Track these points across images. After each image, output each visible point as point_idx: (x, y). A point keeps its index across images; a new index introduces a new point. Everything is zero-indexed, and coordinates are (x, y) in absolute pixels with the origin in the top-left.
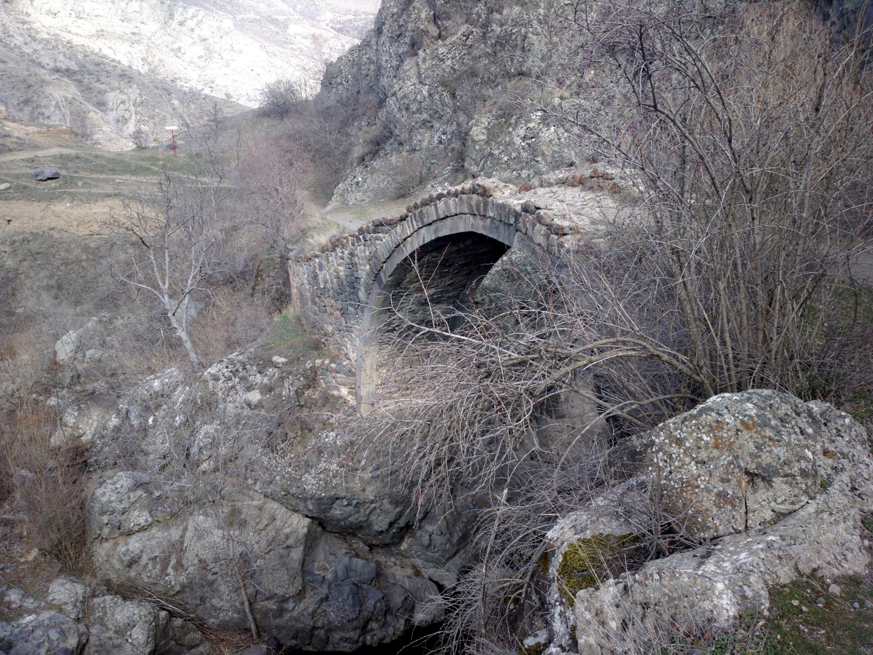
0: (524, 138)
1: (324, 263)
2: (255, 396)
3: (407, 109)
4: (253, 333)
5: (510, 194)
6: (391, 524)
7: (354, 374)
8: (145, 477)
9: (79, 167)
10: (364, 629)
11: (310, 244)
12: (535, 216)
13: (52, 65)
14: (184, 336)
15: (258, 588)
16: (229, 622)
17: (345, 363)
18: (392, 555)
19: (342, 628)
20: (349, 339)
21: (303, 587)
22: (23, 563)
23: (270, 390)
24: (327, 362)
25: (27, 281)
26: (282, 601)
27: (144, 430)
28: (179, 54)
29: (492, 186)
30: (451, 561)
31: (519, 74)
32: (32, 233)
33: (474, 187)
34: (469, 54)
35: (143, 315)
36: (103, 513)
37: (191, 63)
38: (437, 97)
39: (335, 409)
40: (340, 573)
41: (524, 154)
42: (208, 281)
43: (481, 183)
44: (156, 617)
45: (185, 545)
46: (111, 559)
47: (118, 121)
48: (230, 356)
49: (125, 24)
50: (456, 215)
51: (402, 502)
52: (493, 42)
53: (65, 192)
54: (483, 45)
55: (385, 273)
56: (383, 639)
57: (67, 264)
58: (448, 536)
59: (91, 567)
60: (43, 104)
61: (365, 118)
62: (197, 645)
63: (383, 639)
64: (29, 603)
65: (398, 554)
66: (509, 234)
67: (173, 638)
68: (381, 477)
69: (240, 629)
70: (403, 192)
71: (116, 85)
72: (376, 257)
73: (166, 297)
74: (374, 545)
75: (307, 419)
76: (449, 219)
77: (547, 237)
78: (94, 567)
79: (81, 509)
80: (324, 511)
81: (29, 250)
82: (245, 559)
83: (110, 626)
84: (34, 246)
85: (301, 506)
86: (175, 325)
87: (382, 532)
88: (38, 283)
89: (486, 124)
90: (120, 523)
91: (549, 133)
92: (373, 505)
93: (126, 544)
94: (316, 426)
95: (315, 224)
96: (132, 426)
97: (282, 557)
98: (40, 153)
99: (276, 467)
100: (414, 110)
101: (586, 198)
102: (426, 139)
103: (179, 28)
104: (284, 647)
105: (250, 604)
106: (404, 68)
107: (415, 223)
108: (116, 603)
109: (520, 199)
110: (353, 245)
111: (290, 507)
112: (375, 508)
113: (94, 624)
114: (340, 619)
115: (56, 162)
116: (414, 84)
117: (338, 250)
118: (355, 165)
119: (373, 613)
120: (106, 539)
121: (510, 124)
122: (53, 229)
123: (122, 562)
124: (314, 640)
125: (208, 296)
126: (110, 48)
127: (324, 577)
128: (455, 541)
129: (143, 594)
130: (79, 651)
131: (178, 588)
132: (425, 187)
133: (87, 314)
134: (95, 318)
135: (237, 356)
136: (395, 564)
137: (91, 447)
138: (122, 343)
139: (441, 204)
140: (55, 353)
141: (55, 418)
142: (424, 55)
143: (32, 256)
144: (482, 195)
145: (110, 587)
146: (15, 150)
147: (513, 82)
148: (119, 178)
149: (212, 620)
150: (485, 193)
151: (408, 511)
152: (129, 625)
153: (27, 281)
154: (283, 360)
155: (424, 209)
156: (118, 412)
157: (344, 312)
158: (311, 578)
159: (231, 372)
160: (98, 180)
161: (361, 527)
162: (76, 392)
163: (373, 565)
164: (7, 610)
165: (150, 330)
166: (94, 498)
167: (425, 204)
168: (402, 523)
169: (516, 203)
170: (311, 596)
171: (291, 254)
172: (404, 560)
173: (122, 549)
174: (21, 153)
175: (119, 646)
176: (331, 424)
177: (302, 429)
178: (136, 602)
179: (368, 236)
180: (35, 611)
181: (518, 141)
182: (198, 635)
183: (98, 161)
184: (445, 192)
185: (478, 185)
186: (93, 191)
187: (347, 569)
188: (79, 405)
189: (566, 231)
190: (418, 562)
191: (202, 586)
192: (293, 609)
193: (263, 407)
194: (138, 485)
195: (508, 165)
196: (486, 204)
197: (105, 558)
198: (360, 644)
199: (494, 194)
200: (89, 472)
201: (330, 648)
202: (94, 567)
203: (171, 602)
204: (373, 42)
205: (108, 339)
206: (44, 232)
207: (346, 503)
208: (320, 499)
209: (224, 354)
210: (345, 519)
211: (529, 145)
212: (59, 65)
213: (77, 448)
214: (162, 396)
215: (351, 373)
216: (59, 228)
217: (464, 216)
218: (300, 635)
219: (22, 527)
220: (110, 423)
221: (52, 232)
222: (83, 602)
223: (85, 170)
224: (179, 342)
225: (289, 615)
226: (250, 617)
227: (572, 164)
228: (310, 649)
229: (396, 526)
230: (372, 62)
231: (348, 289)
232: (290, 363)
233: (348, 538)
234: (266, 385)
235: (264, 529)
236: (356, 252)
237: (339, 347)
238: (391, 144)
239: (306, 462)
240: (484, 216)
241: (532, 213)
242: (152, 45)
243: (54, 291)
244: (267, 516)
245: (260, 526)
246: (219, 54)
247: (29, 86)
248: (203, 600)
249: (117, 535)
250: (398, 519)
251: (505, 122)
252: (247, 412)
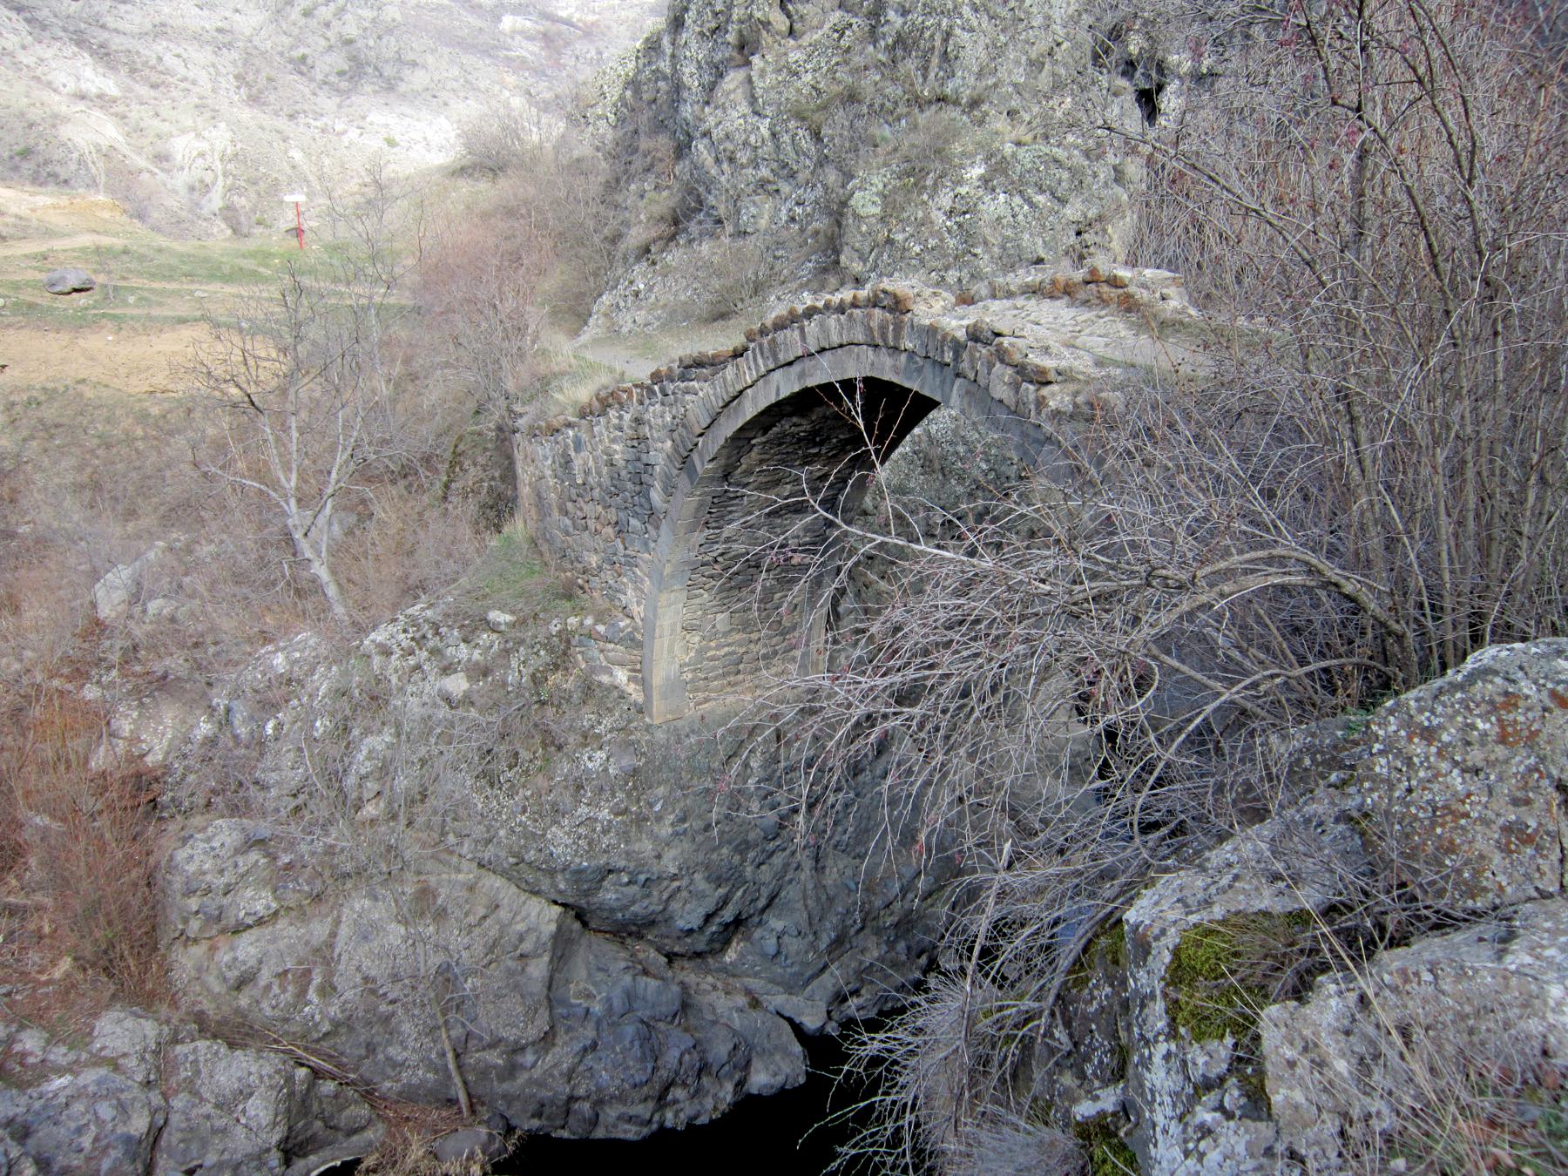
0: (950, 213)
1: (584, 436)
2: (457, 684)
3: (731, 160)
4: (450, 567)
5: (944, 308)
6: (708, 918)
7: (639, 645)
8: (264, 828)
9: (129, 270)
10: (661, 1100)
11: (557, 402)
12: (993, 349)
13: (72, 86)
14: (321, 571)
15: (470, 1027)
16: (419, 1087)
17: (622, 624)
18: (709, 972)
19: (621, 1098)
20: (631, 580)
21: (552, 1028)
22: (47, 983)
23: (486, 673)
24: (589, 621)
25: (37, 477)
26: (514, 1051)
27: (259, 744)
28: (304, 69)
29: (911, 293)
30: (815, 983)
31: (939, 100)
32: (44, 389)
33: (876, 296)
34: (846, 63)
35: (250, 539)
36: (189, 892)
37: (325, 83)
38: (786, 138)
39: (604, 709)
40: (617, 1003)
41: (951, 243)
42: (365, 473)
43: (889, 288)
44: (290, 1079)
45: (337, 951)
46: (204, 976)
47: (192, 189)
48: (410, 611)
49: (206, 12)
50: (841, 346)
51: (728, 880)
52: (890, 41)
53: (104, 315)
54: (871, 48)
55: (701, 455)
56: (696, 1117)
57: (108, 446)
58: (811, 937)
59: (168, 990)
60: (56, 157)
61: (651, 177)
62: (363, 1129)
63: (696, 1117)
64: (60, 1054)
65: (719, 970)
66: (943, 382)
67: (320, 1116)
68: (689, 832)
69: (438, 1100)
70: (724, 309)
71: (189, 123)
72: (684, 426)
73: (293, 502)
74: (676, 954)
75: (553, 727)
76: (828, 353)
77: (1016, 387)
78: (174, 990)
79: (149, 884)
80: (587, 893)
81: (40, 420)
82: (446, 977)
83: (207, 1095)
84: (49, 413)
85: (545, 885)
86: (309, 554)
87: (691, 931)
88: (57, 480)
89: (881, 186)
90: (221, 908)
91: (995, 205)
92: (676, 884)
93: (232, 949)
94: (571, 740)
95: (564, 367)
96: (236, 737)
97: (510, 973)
98: (58, 244)
99: (500, 813)
100: (744, 161)
101: (1080, 319)
102: (762, 214)
103: (302, 21)
104: (519, 1132)
105: (457, 1056)
106: (725, 87)
107: (760, 361)
108: (216, 1053)
109: (962, 318)
110: (642, 403)
111: (523, 885)
112: (679, 888)
113: (176, 1092)
114: (618, 1082)
115: (87, 261)
116: (744, 116)
117: (612, 413)
118: (631, 260)
119: (677, 1073)
120: (195, 941)
121: (925, 187)
122: (83, 381)
123: (225, 980)
124: (571, 1120)
125: (363, 502)
126: (178, 56)
127: (588, 1010)
128: (823, 946)
129: (264, 1038)
130: (151, 1139)
131: (326, 1027)
132: (764, 300)
133: (145, 536)
134: (161, 544)
135: (423, 609)
136: (715, 988)
137: (164, 774)
138: (212, 587)
139: (812, 327)
140: (94, 605)
141: (98, 721)
142: (762, 64)
143: (46, 430)
144: (891, 310)
145: (204, 1026)
146: (12, 237)
147: (928, 113)
148: (202, 290)
149: (388, 1084)
150: (898, 306)
151: (739, 893)
152: (241, 1092)
153: (37, 477)
154: (509, 618)
155: (780, 336)
156: (212, 710)
157: (621, 530)
158: (564, 1011)
159: (413, 639)
160: (162, 293)
161: (653, 923)
162: (134, 674)
163: (675, 989)
164: (18, 1068)
165: (262, 563)
166: (172, 867)
167: (780, 325)
168: (728, 915)
169: (956, 324)
170: (565, 1043)
171: (521, 422)
172: (731, 980)
173: (224, 957)
174: (22, 244)
175: (224, 1131)
176: (599, 736)
177: (545, 745)
178: (251, 1052)
179: (670, 387)
180: (72, 1069)
181: (939, 218)
182: (364, 1111)
183: (162, 259)
184: (820, 304)
185: (884, 292)
186: (156, 312)
187: (630, 996)
188: (140, 699)
189: (1052, 376)
190: (755, 984)
191: (369, 1023)
192: (534, 1066)
193: (472, 704)
194: (253, 843)
195: (922, 262)
196: (898, 328)
197: (193, 973)
198: (655, 1126)
199: (914, 307)
200: (161, 819)
201: (600, 1133)
202: (174, 990)
203: (315, 1052)
204: (666, 41)
205: (187, 580)
206: (67, 387)
207: (626, 880)
208: (580, 872)
209: (395, 607)
210: (624, 908)
211: (960, 225)
212: (84, 86)
213: (139, 776)
214: (289, 681)
215: (632, 642)
216: (94, 379)
217: (856, 349)
218: (547, 1111)
219: (41, 918)
220: (197, 732)
221: (80, 387)
222: (156, 1053)
223: (140, 274)
224: (316, 586)
225: (526, 1076)
226: (457, 1080)
227: (1040, 261)
228: (565, 1134)
229: (717, 920)
230: (665, 78)
231: (629, 485)
232: (521, 623)
233: (629, 941)
234: (477, 663)
235: (479, 924)
236: (646, 417)
237: (613, 593)
238: (700, 223)
239: (554, 804)
240: (896, 348)
241: (987, 344)
242: (255, 52)
243: (88, 494)
244: (484, 901)
245: (472, 919)
246: (376, 68)
247: (31, 126)
248: (371, 1048)
249: (214, 932)
250: (721, 909)
251: (915, 184)
252: (443, 712)
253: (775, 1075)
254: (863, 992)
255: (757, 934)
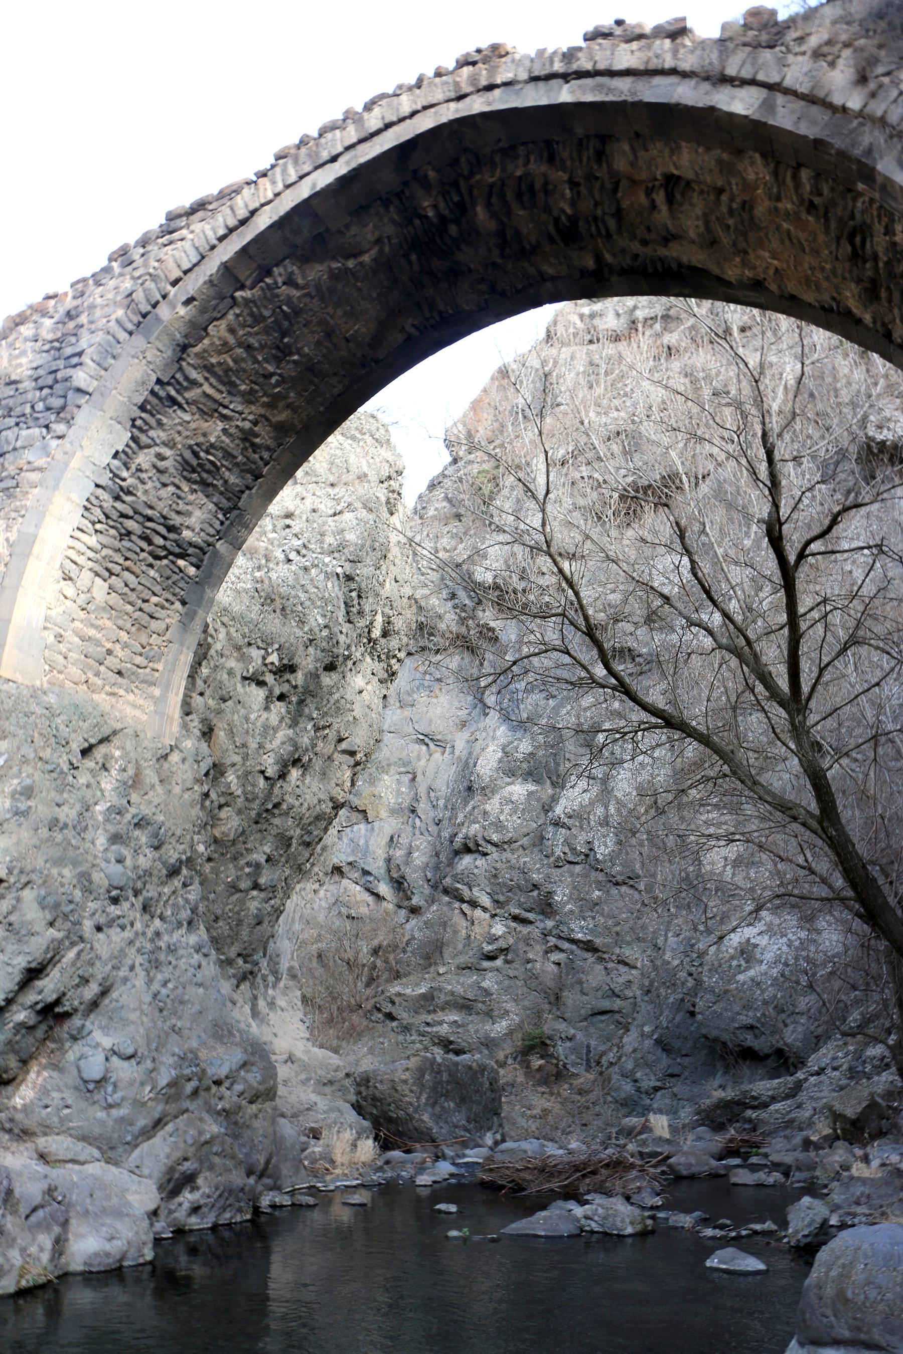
30: (145, 1147)
58: (149, 1064)
253: (111, 1239)
254: (200, 1181)
255: (73, 1053)
